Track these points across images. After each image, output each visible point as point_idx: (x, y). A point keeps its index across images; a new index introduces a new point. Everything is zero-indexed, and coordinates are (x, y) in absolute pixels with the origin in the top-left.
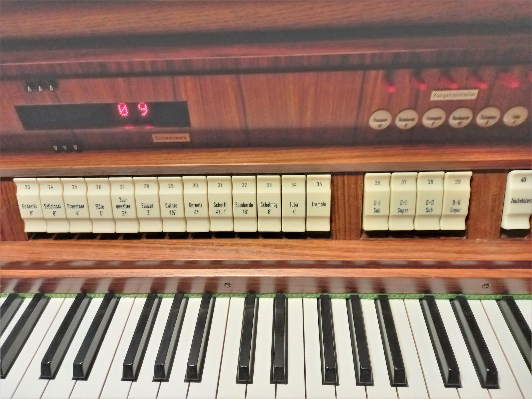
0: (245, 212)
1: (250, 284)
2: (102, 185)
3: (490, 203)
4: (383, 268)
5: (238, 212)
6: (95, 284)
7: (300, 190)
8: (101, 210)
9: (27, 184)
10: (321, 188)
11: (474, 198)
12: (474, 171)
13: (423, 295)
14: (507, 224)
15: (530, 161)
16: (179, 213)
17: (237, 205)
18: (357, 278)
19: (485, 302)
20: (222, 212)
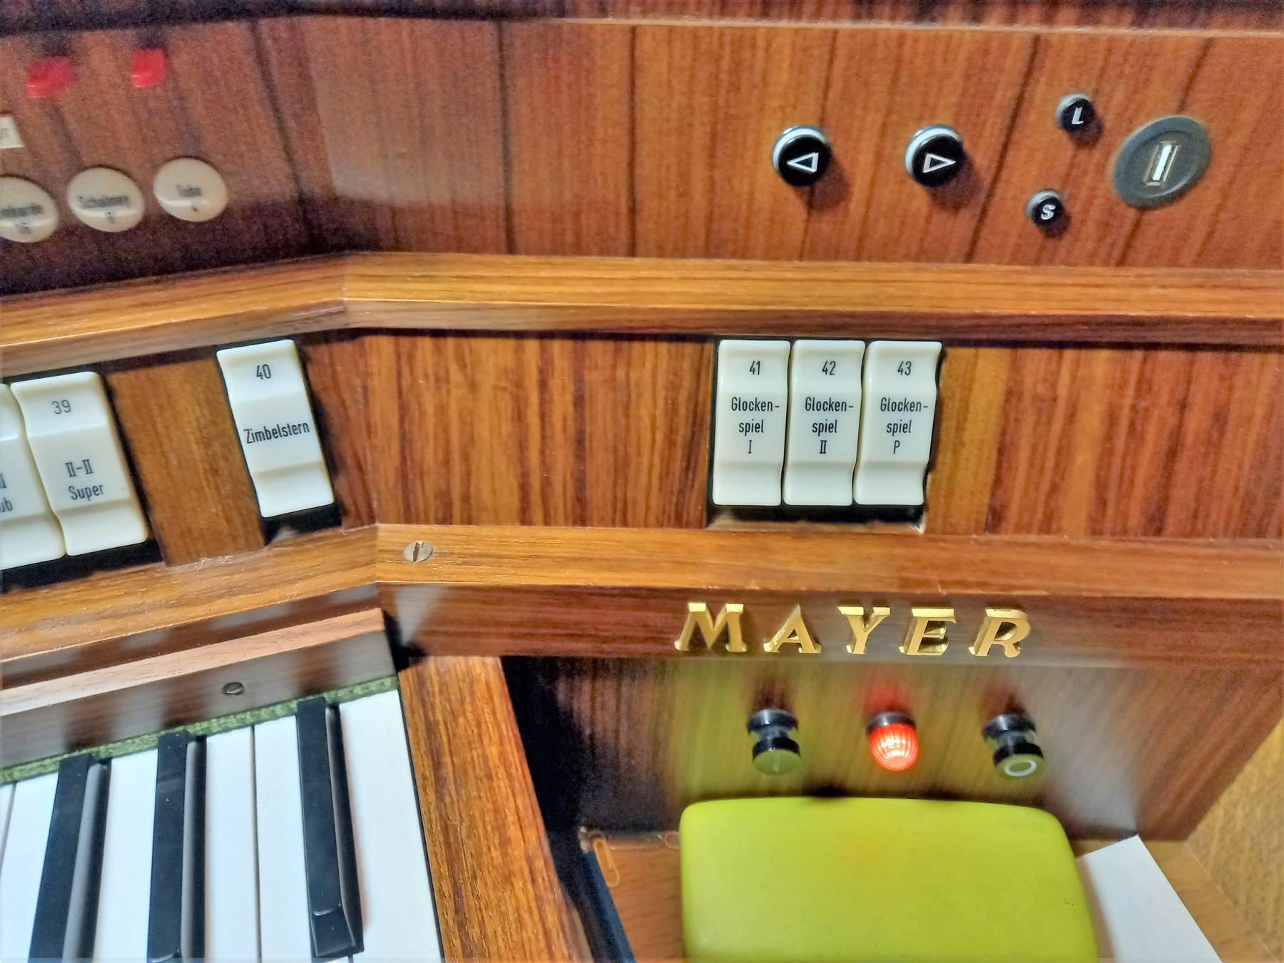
3: (197, 451)
4: (61, 676)
10: (79, 421)
11: (141, 445)
14: (272, 505)
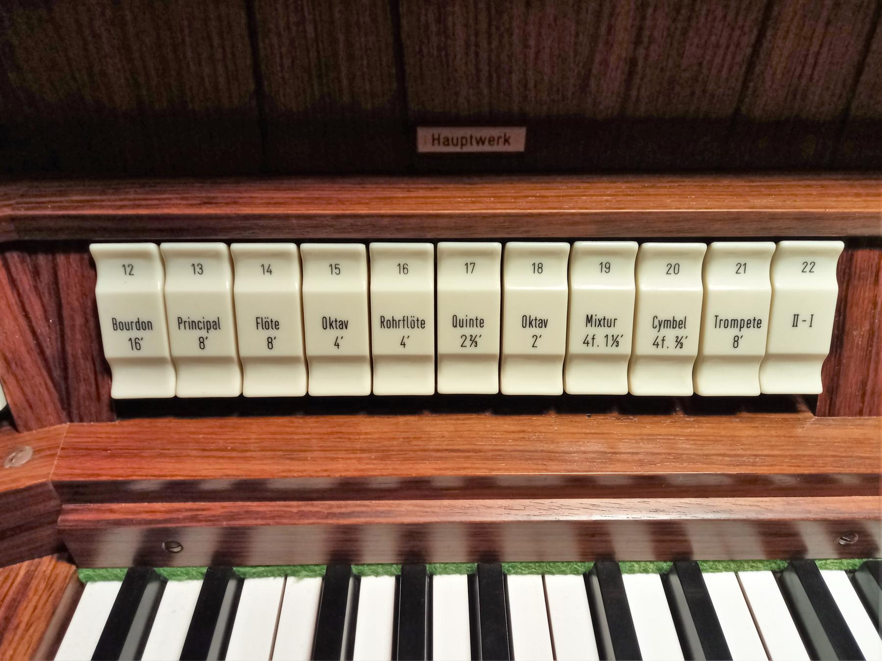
0: (136, 343)
1: (225, 541)
2: (412, 264)
6: (357, 541)
8: (271, 333)
9: (127, 262)
13: (857, 562)
15: (879, 213)
16: (289, 343)
17: (388, 323)
18: (794, 520)
19: (747, 576)
20: (600, 340)
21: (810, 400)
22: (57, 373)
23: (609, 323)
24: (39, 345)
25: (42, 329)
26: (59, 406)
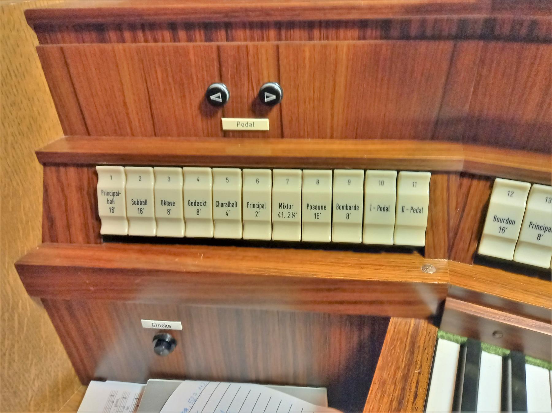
0: (317, 216)
5: (249, 214)
7: (389, 189)
10: (417, 189)
12: (433, 172)
17: (221, 205)
20: (286, 215)
21: (421, 251)
22: (451, 235)
23: (291, 207)
24: (449, 220)
25: (453, 213)
26: (447, 249)
